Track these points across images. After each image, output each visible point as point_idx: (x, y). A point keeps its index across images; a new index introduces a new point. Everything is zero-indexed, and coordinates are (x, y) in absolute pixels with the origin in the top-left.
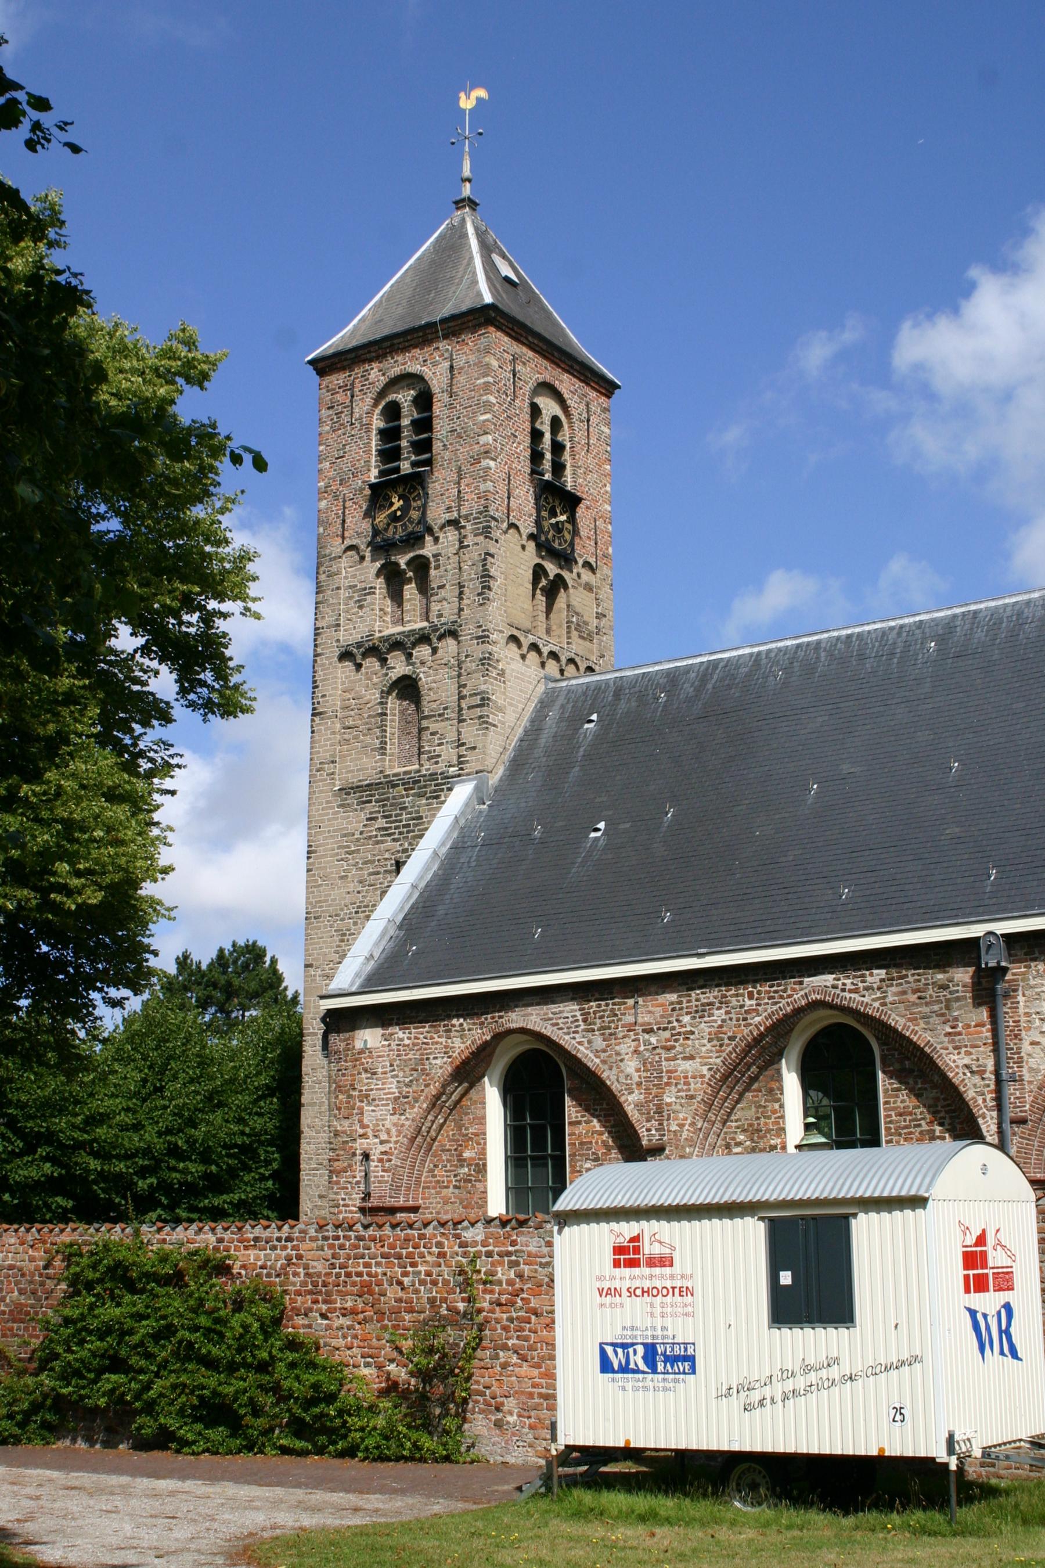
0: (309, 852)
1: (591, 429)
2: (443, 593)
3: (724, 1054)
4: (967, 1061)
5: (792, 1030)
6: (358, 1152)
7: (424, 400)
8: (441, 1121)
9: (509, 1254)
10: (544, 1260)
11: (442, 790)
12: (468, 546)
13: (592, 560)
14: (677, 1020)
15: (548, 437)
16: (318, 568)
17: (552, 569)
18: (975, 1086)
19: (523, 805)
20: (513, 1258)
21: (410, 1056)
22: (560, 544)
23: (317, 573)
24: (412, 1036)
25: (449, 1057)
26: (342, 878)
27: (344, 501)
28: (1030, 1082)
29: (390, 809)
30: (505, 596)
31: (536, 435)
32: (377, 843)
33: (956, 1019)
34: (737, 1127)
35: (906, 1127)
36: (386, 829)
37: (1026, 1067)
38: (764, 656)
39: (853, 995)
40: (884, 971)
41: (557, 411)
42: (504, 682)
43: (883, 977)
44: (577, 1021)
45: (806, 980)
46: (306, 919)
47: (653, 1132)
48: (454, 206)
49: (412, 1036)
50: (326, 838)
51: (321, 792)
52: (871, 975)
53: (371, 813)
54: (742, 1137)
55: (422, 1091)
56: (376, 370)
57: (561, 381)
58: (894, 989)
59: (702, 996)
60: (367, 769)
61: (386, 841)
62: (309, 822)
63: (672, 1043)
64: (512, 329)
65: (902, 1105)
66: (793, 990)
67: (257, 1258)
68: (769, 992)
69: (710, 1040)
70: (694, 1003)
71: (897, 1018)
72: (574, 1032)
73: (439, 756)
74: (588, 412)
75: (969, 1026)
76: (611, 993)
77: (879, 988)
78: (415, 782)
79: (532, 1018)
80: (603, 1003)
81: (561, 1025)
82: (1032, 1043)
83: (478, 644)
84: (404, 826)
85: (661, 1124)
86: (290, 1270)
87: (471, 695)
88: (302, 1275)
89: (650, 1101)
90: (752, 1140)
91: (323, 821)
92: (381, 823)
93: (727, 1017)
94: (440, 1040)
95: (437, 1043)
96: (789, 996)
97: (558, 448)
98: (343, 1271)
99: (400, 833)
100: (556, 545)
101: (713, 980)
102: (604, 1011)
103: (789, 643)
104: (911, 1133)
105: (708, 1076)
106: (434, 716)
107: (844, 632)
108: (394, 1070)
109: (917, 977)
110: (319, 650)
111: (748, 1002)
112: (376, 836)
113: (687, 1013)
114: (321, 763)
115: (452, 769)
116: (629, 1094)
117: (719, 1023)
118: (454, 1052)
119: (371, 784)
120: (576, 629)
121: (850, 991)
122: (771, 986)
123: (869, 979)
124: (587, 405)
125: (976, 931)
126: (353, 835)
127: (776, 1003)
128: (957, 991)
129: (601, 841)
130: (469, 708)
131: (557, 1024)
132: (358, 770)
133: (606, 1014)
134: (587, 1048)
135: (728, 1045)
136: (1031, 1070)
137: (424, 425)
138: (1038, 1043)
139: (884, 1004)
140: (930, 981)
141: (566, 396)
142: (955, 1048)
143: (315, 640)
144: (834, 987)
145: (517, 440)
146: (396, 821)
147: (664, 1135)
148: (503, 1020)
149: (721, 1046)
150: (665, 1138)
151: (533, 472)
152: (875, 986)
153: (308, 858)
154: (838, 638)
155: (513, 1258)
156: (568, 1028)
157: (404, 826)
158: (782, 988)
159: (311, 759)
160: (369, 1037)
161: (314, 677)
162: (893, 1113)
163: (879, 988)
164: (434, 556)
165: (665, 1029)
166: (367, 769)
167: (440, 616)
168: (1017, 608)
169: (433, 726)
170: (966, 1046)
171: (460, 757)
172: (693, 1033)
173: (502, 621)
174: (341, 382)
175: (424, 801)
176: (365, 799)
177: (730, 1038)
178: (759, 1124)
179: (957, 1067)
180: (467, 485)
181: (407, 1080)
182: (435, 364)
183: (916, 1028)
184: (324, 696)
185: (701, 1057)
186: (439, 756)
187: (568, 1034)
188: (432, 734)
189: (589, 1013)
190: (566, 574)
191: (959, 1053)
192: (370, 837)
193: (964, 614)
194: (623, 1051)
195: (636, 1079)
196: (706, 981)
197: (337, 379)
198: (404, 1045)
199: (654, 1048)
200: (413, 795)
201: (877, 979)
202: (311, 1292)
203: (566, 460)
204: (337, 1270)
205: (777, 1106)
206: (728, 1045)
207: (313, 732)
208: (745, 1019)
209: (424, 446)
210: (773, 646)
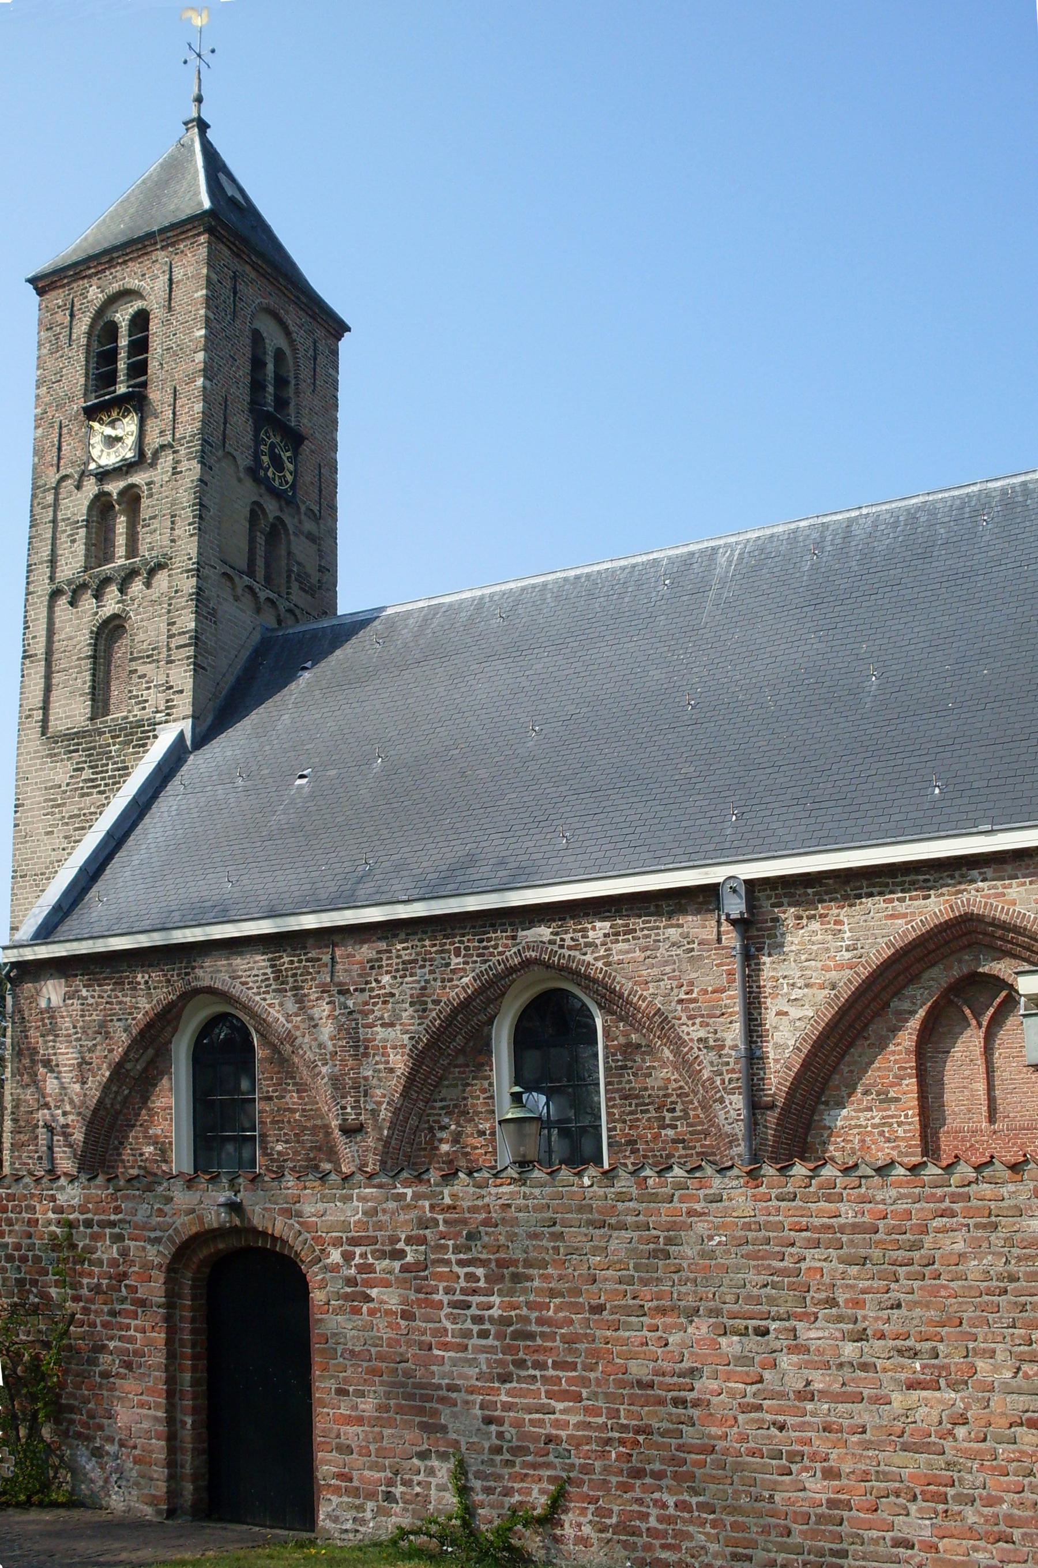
0: (16, 806)
1: (318, 370)
2: (155, 524)
3: (427, 1021)
4: (702, 1034)
5: (503, 994)
6: (41, 1123)
7: (141, 320)
8: (126, 1092)
9: (113, 1224)
10: (153, 1235)
11: (148, 738)
12: (181, 472)
13: (316, 508)
14: (376, 981)
15: (270, 367)
16: (32, 501)
17: (271, 507)
18: (712, 1063)
19: (229, 753)
20: (117, 1230)
21: (94, 1017)
22: (281, 484)
23: (32, 506)
24: (96, 994)
25: (133, 1019)
26: (48, 833)
27: (61, 428)
28: (776, 1061)
29: (96, 758)
30: (219, 529)
31: (257, 364)
32: (83, 795)
33: (691, 983)
34: (442, 1108)
35: (631, 1113)
36: (92, 780)
37: (772, 1043)
38: (487, 600)
39: (572, 953)
40: (608, 924)
41: (282, 343)
42: (215, 623)
43: (606, 931)
44: (268, 979)
45: (521, 933)
46: (13, 877)
47: (349, 1110)
48: (185, 127)
49: (96, 994)
50: (33, 790)
51: (29, 740)
52: (594, 929)
53: (77, 763)
54: (447, 1120)
55: (106, 1056)
56: (94, 287)
57: (287, 312)
58: (621, 946)
60: (75, 716)
61: (91, 794)
62: (17, 774)
63: (370, 1007)
64: (234, 244)
65: (628, 1086)
66: (506, 946)
68: (479, 948)
69: (412, 1004)
70: (395, 961)
71: (624, 981)
72: (264, 993)
73: (146, 701)
74: (314, 350)
75: (706, 992)
76: (305, 948)
77: (603, 944)
78: (121, 730)
79: (212, 973)
80: (296, 959)
81: (251, 984)
82: (779, 1013)
83: (188, 578)
84: (110, 777)
85: (358, 1101)
87: (180, 634)
89: (346, 1074)
91: (30, 772)
92: (87, 774)
93: (431, 977)
94: (124, 999)
95: (120, 1003)
96: (500, 954)
97: (281, 382)
99: (106, 785)
100: (277, 484)
101: (416, 933)
102: (296, 968)
103: (512, 585)
104: (638, 1120)
105: (409, 1047)
106: (142, 657)
107: (572, 573)
108: (76, 1033)
109: (646, 932)
110: (32, 589)
111: (455, 960)
112: (82, 788)
113: (387, 972)
114: (30, 710)
115: (158, 715)
116: (323, 1065)
117: (423, 984)
118: (138, 1013)
119: (79, 732)
120: (296, 580)
121: (570, 948)
122: (481, 941)
123: (591, 933)
124: (315, 342)
125: (714, 875)
126: (60, 787)
127: (486, 961)
128: (692, 950)
129: (306, 789)
130: (178, 648)
131: (247, 983)
132: (67, 717)
133: (299, 972)
134: (278, 1012)
136: (777, 1046)
137: (139, 346)
138: (786, 1014)
139: (608, 964)
140: (661, 938)
141: (292, 328)
142: (689, 1018)
143: (28, 577)
144: (552, 942)
145: (237, 364)
146: (102, 772)
147: (360, 1114)
148: (190, 977)
149: (424, 1010)
150: (362, 1117)
151: (253, 402)
152: (598, 942)
153: (16, 812)
154: (566, 579)
155: (117, 1230)
156: (259, 987)
157: (110, 777)
158: (493, 943)
159: (21, 706)
160: (52, 992)
161: (25, 617)
162: (617, 1095)
163: (603, 944)
164: (148, 484)
165: (363, 990)
166: (75, 716)
167: (151, 549)
168: (760, 542)
169: (142, 669)
170: (702, 1016)
171: (167, 701)
173: (214, 555)
174: (60, 302)
175: (131, 750)
176: (72, 748)
178: (465, 1105)
179: (691, 1040)
180: (183, 406)
181: (90, 1044)
182: (154, 278)
183: (645, 993)
184: (34, 637)
185: (401, 1024)
186: (146, 701)
187: (259, 994)
188: (140, 677)
189: (281, 971)
190: (288, 520)
191: (694, 1024)
192: (76, 789)
193: (701, 551)
194: (316, 1016)
195: (331, 1048)
196: (407, 935)
197: (57, 298)
198: (88, 1005)
199: (351, 1013)
200: (120, 743)
201: (601, 933)
203: (289, 398)
205: (486, 1084)
207: (23, 676)
209: (139, 369)
210: (497, 588)
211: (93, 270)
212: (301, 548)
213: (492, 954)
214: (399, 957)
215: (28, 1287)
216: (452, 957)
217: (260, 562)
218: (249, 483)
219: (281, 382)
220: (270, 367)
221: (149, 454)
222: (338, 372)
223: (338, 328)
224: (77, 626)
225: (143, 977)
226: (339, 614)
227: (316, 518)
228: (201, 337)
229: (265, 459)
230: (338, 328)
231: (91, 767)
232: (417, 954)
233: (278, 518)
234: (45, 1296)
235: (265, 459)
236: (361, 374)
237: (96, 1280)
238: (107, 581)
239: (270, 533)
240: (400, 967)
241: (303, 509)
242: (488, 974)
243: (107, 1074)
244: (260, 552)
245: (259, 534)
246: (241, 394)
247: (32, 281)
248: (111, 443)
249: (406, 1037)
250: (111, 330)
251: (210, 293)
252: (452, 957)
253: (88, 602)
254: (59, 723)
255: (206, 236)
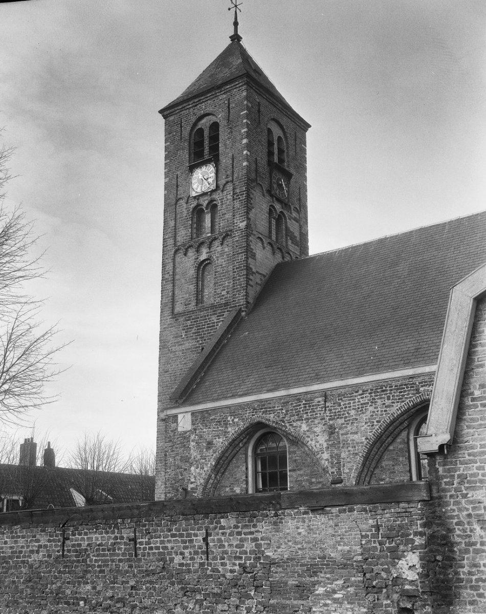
3: (374, 430)
7: (215, 126)
9: (252, 533)
17: (278, 207)
27: (177, 177)
31: (270, 144)
59: (361, 400)
67: (97, 539)
69: (366, 423)
86: (116, 547)
88: (123, 550)
90: (390, 478)
93: (376, 410)
98: (147, 546)
102: (308, 410)
127: (403, 402)
135: (376, 425)
149: (373, 425)
157: (206, 331)
172: (357, 419)
177: (377, 422)
189: (300, 411)
190: (285, 212)
202: (129, 560)
204: (144, 546)
206: (376, 425)
208: (385, 411)
211: (190, 106)
212: (293, 226)
213: (406, 398)
214: (359, 402)
215: (206, 567)
216: (386, 401)
217: (274, 232)
218: (268, 198)
219: (281, 151)
220: (276, 146)
221: (221, 187)
222: (306, 146)
223: (306, 126)
224: (187, 264)
225: (231, 418)
226: (309, 255)
227: (298, 212)
228: (244, 132)
229: (275, 186)
230: (306, 126)
231: (196, 327)
232: (369, 400)
233: (281, 212)
234: (215, 570)
235: (275, 186)
236: (315, 147)
237: (243, 562)
238: (202, 243)
239: (278, 218)
240: (360, 406)
241: (292, 207)
242: (404, 407)
243: (213, 463)
244: (274, 227)
245: (273, 219)
246: (263, 161)
247: (161, 112)
248: (202, 179)
249: (364, 438)
250: (201, 131)
251: (248, 112)
252: (386, 401)
253: (191, 253)
254: (179, 308)
255: (245, 86)
